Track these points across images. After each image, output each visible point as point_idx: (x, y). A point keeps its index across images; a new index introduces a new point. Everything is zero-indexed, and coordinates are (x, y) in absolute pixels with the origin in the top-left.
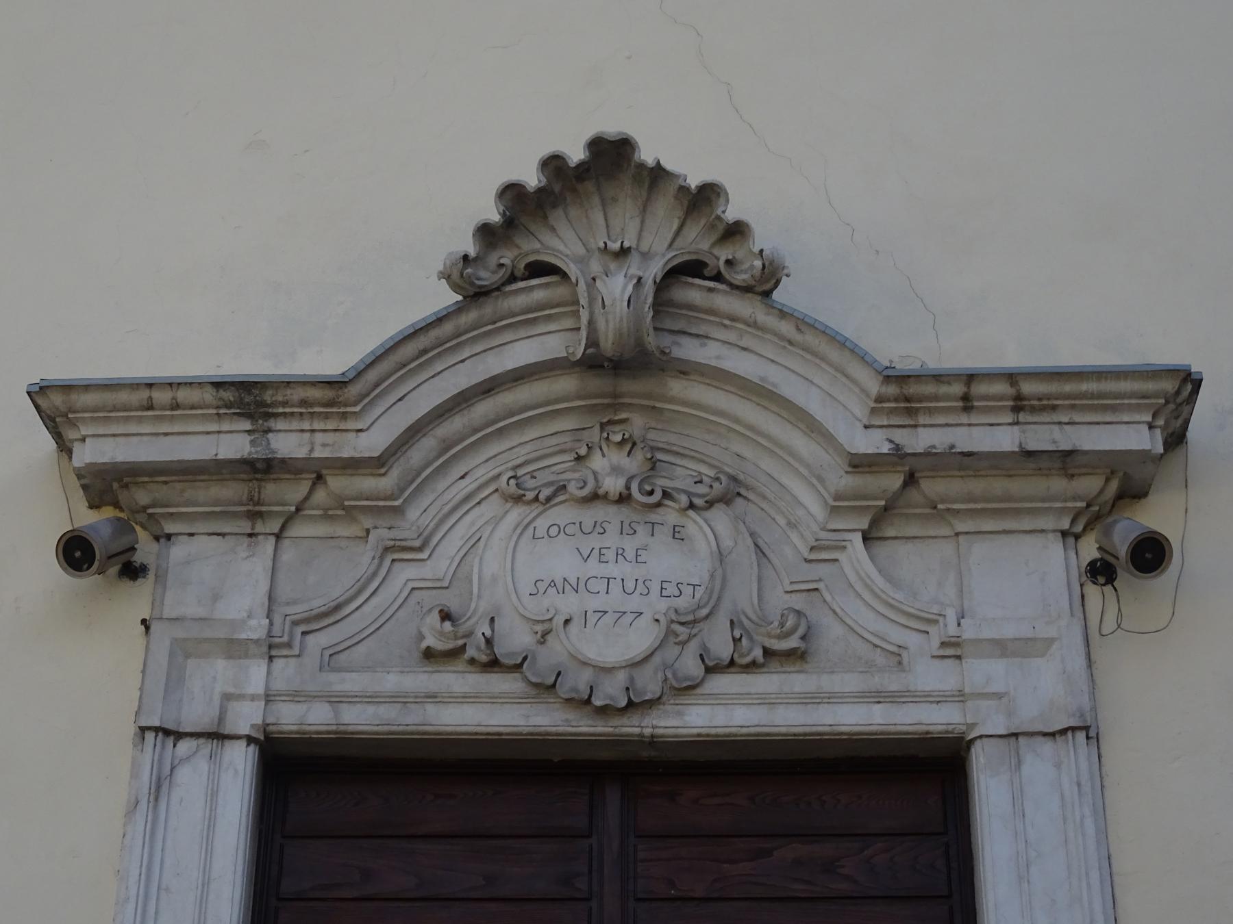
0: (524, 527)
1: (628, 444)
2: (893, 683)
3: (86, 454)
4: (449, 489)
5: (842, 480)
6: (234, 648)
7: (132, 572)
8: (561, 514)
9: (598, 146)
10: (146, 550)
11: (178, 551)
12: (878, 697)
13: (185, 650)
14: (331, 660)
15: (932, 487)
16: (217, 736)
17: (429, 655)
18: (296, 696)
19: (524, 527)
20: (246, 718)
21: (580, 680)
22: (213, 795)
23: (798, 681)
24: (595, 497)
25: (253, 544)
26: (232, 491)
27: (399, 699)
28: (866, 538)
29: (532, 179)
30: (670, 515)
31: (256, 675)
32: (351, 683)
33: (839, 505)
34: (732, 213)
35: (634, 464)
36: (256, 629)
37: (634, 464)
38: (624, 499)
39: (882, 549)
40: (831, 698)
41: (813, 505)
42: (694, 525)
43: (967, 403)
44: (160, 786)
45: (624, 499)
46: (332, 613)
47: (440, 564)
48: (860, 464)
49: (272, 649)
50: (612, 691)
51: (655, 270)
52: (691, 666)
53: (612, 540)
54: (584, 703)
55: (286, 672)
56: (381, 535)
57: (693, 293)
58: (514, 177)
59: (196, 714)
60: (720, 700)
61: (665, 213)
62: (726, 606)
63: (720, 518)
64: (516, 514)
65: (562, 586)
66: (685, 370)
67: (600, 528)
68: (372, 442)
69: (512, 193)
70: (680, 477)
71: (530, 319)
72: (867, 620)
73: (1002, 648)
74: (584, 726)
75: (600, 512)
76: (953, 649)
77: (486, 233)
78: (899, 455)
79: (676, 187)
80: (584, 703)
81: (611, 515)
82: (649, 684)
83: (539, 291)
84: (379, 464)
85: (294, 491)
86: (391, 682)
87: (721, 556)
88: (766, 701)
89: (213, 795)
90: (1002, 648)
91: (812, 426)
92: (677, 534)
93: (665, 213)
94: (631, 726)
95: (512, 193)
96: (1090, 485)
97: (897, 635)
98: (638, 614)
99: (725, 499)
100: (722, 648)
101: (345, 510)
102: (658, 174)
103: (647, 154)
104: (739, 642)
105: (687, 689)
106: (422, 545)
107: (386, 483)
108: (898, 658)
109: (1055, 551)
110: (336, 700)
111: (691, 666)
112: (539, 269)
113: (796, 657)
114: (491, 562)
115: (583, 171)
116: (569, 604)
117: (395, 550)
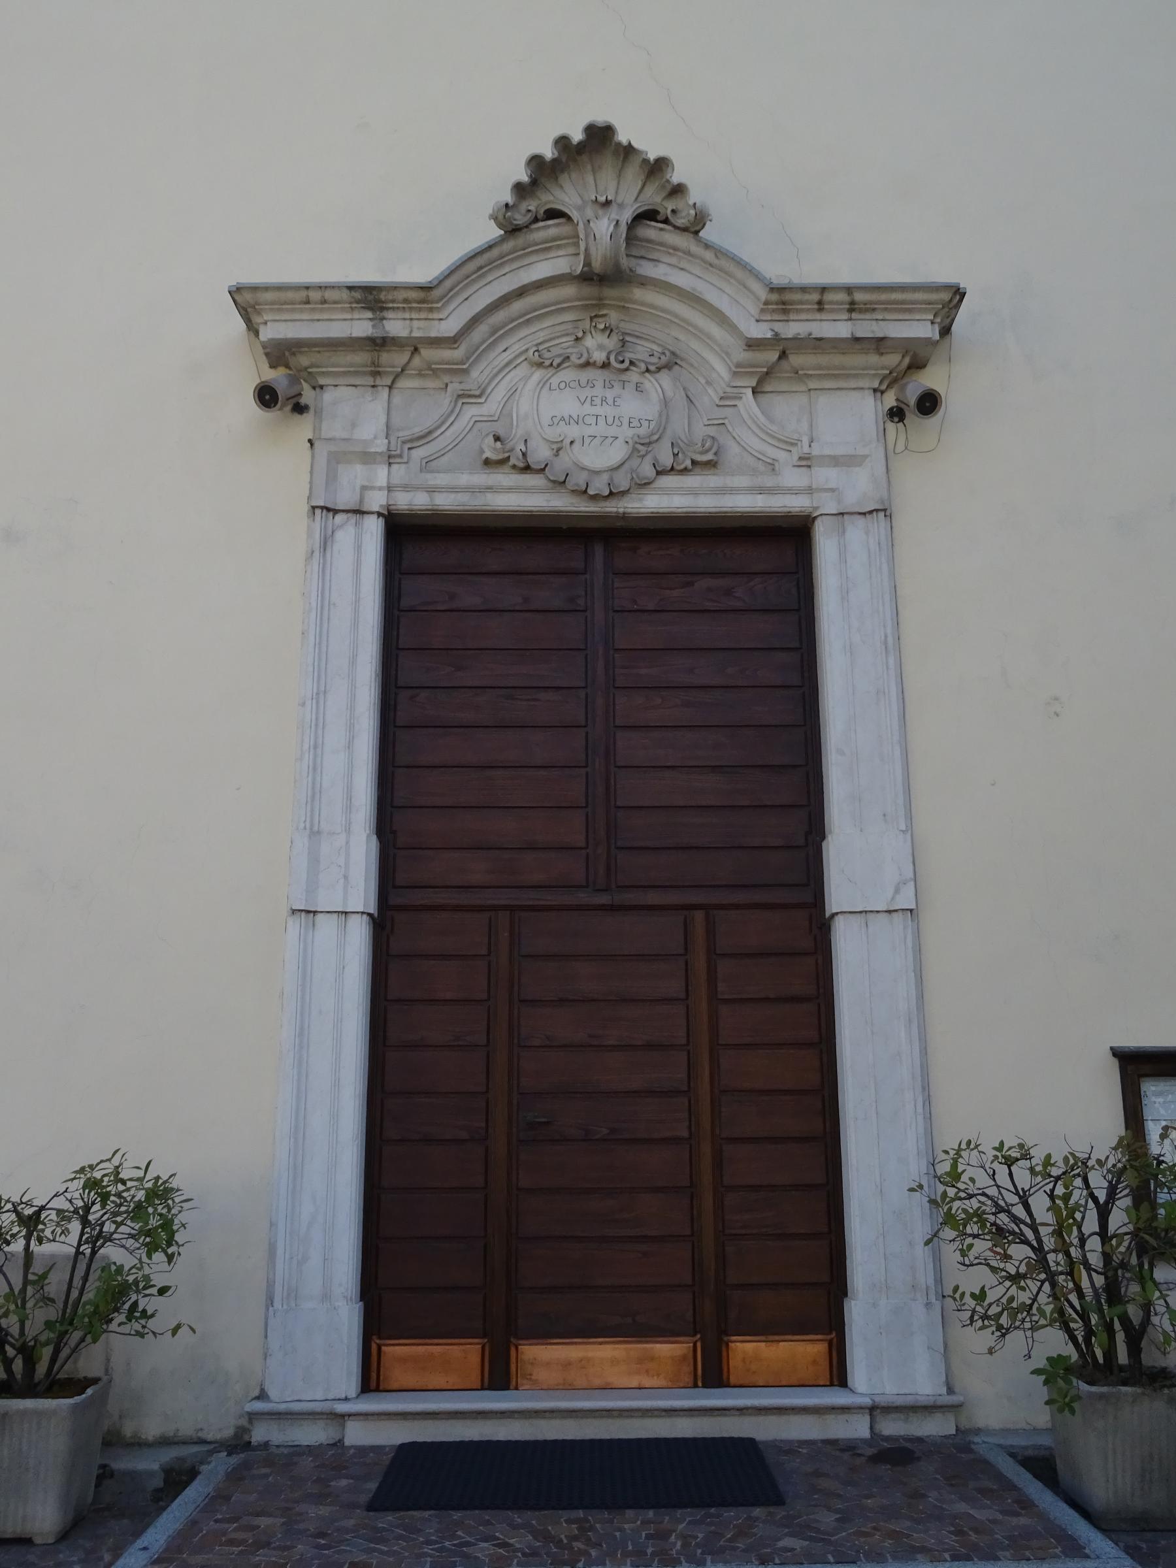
0: (543, 383)
2: (769, 482)
3: (269, 332)
5: (741, 355)
6: (367, 458)
7: (299, 409)
8: (567, 375)
11: (328, 396)
12: (761, 490)
13: (337, 459)
14: (427, 465)
15: (795, 360)
16: (359, 512)
17: (487, 462)
18: (406, 488)
19: (543, 383)
20: (377, 501)
21: (579, 479)
22: (358, 548)
23: (713, 480)
24: (587, 364)
26: (361, 358)
27: (470, 490)
29: (549, 153)
30: (634, 376)
31: (381, 475)
32: (441, 479)
33: (739, 371)
34: (676, 178)
35: (611, 343)
36: (380, 445)
37: (611, 343)
38: (605, 365)
40: (732, 491)
41: (722, 370)
42: (649, 383)
43: (820, 306)
44: (326, 542)
46: (425, 436)
47: (491, 406)
48: (753, 344)
49: (390, 459)
50: (599, 486)
51: (627, 215)
52: (648, 470)
55: (399, 473)
56: (455, 387)
57: (650, 231)
59: (345, 497)
63: (665, 378)
64: (538, 374)
65: (568, 420)
66: (644, 282)
68: (449, 326)
70: (640, 351)
71: (546, 248)
72: (754, 443)
73: (835, 461)
75: (591, 373)
76: (806, 461)
79: (641, 159)
82: (622, 482)
83: (552, 229)
85: (399, 358)
86: (464, 479)
87: (666, 402)
88: (693, 492)
89: (358, 548)
90: (835, 461)
92: (638, 387)
97: (772, 453)
99: (668, 366)
100: (667, 460)
101: (432, 371)
103: (622, 137)
105: (646, 484)
107: (458, 353)
110: (431, 490)
111: (648, 470)
112: (553, 214)
113: (711, 465)
114: (524, 404)
115: (581, 147)
116: (573, 431)
117: (465, 397)
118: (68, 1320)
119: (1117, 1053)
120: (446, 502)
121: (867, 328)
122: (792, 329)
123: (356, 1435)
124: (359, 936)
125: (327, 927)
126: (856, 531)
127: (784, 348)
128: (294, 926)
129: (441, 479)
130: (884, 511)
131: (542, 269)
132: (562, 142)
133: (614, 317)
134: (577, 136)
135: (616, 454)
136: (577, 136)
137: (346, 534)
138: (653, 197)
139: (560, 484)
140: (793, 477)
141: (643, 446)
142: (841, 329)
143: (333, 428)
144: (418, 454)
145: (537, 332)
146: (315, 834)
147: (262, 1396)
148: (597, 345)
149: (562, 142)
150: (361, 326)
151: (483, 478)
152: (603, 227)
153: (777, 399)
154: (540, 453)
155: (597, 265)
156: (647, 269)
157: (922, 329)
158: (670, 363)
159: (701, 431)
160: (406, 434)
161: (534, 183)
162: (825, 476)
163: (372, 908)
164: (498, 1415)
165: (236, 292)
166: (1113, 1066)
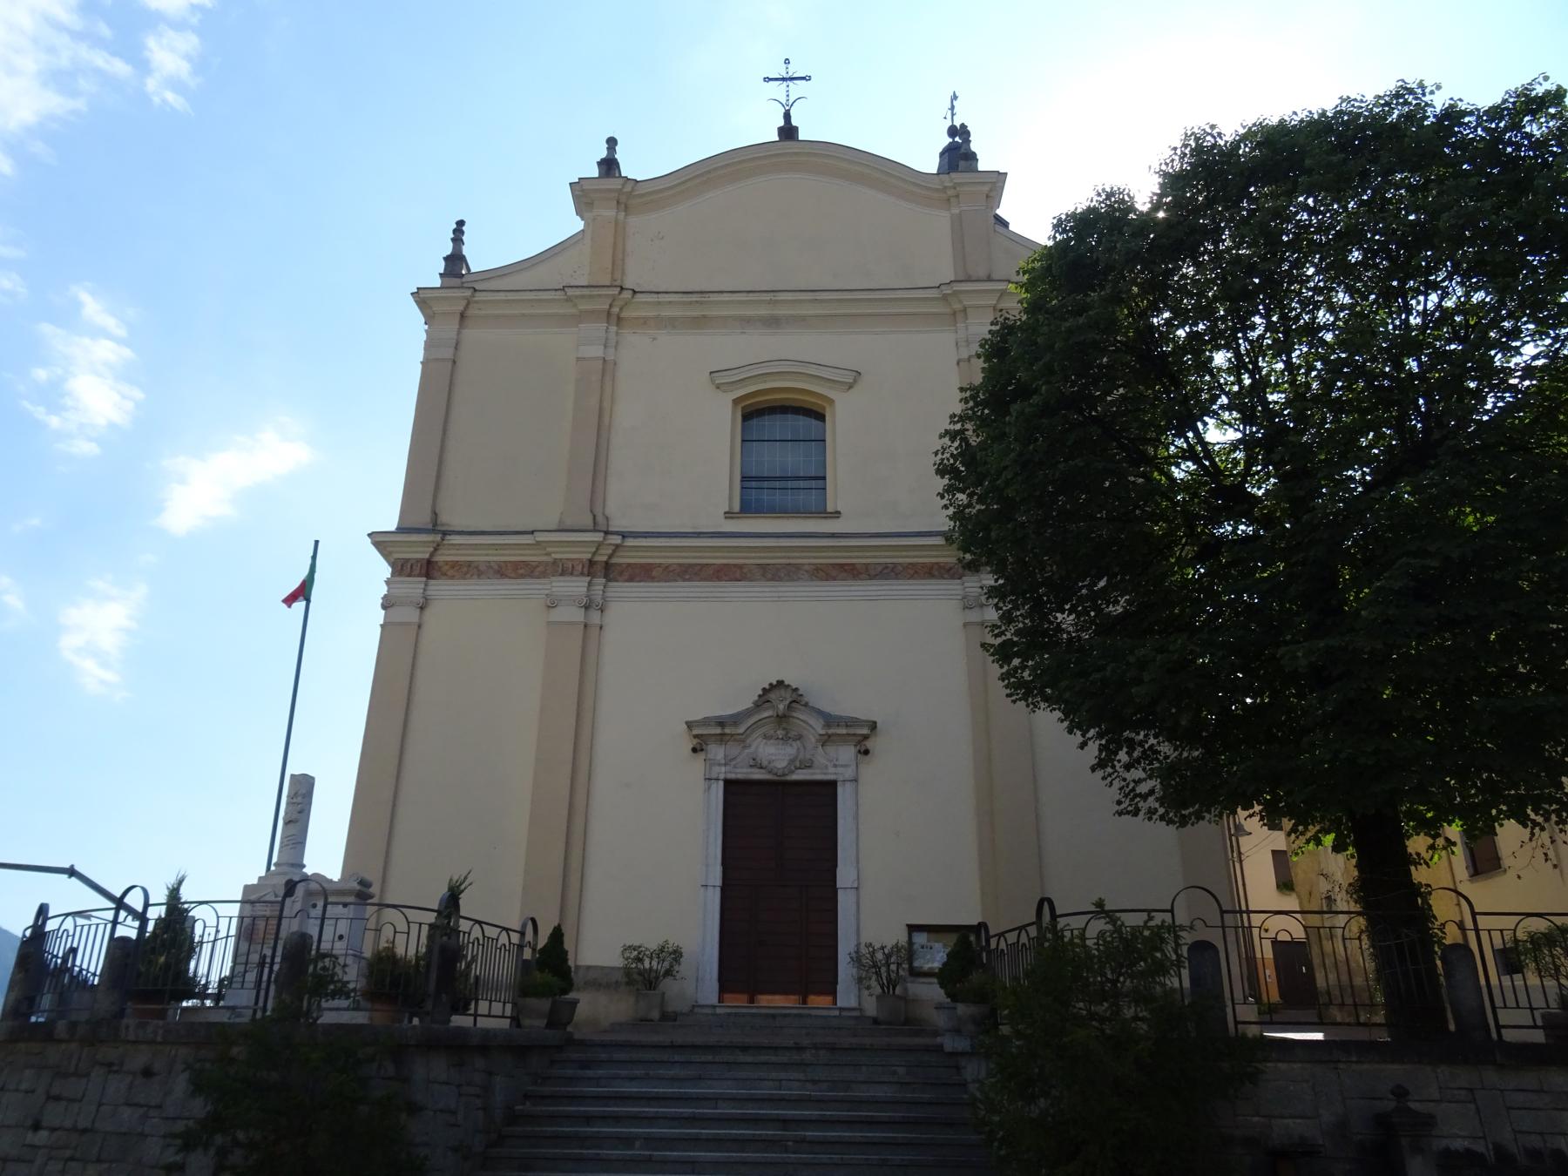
0: (766, 743)
1: (784, 729)
2: (825, 771)
3: (695, 732)
4: (754, 735)
5: (818, 737)
6: (720, 765)
7: (702, 750)
9: (778, 681)
10: (704, 747)
11: (709, 747)
12: (825, 774)
13: (711, 765)
14: (735, 767)
15: (832, 738)
16: (717, 779)
17: (751, 766)
18: (730, 772)
19: (766, 743)
20: (722, 776)
21: (775, 770)
23: (810, 771)
25: (1180, 788)
26: (719, 737)
27: (747, 773)
28: (822, 746)
29: (767, 687)
30: (790, 741)
31: (723, 769)
32: (738, 770)
33: (818, 741)
34: (800, 693)
35: (783, 732)
36: (723, 762)
37: (783, 732)
38: (782, 739)
39: (824, 747)
41: (813, 740)
42: (794, 744)
43: (838, 726)
44: (709, 788)
45: (782, 739)
47: (752, 749)
49: (725, 765)
50: (780, 772)
51: (788, 702)
52: (793, 768)
53: (780, 747)
54: (776, 774)
55: (728, 768)
56: (742, 745)
57: (794, 705)
58: (466, 224)
59: (714, 775)
60: (798, 774)
61: (789, 691)
62: (799, 759)
63: (798, 742)
64: (765, 741)
65: (772, 754)
66: (793, 717)
67: (778, 744)
68: (741, 730)
69: (764, 689)
70: (792, 734)
71: (767, 709)
73: (842, 766)
74: (775, 778)
76: (835, 766)
77: (760, 696)
78: (827, 734)
80: (776, 774)
81: (781, 742)
82: (786, 771)
83: (767, 704)
84: (742, 734)
85: (728, 738)
86: (745, 770)
87: (798, 749)
90: (842, 766)
91: (813, 728)
93: (789, 691)
94: (783, 778)
95: (764, 689)
96: (859, 738)
98: (63, 917)
99: (799, 739)
100: (798, 765)
101: (735, 740)
102: (789, 686)
103: (786, 683)
104: (669, 980)
106: (750, 746)
107: (743, 737)
108: (826, 767)
109: (852, 748)
110: (736, 773)
112: (768, 701)
113: (809, 767)
114: (761, 750)
115: (776, 685)
116: (774, 758)
117: (745, 747)
118: (872, 957)
119: (908, 925)
120: (740, 776)
121: (852, 731)
122: (831, 731)
123: (719, 1011)
124: (718, 891)
125: (710, 890)
126: (848, 785)
127: (829, 736)
128: (702, 889)
129: (738, 770)
130: (856, 780)
131: (766, 714)
132: (771, 684)
133: (784, 725)
134: (775, 683)
135: (784, 764)
136: (775, 683)
137: (714, 786)
138: (794, 696)
139: (770, 772)
140: (832, 770)
141: (792, 761)
142: (844, 731)
143: (710, 756)
144: (734, 763)
145: (763, 730)
146: (707, 866)
147: (696, 1002)
148: (780, 733)
149: (771, 684)
150: (718, 731)
151: (749, 770)
152: (781, 707)
153: (828, 747)
154: (765, 763)
155: (780, 714)
156: (795, 714)
157: (865, 731)
158: (800, 737)
159: (808, 757)
160: (729, 758)
161: (764, 694)
162: (840, 770)
163: (721, 885)
164: (448, 353)
165: (687, 723)
166: (906, 929)
